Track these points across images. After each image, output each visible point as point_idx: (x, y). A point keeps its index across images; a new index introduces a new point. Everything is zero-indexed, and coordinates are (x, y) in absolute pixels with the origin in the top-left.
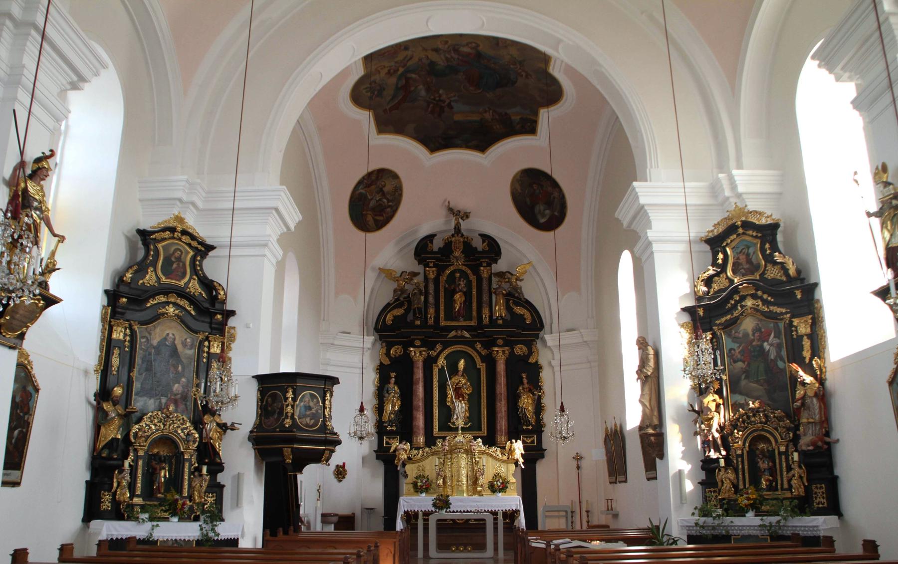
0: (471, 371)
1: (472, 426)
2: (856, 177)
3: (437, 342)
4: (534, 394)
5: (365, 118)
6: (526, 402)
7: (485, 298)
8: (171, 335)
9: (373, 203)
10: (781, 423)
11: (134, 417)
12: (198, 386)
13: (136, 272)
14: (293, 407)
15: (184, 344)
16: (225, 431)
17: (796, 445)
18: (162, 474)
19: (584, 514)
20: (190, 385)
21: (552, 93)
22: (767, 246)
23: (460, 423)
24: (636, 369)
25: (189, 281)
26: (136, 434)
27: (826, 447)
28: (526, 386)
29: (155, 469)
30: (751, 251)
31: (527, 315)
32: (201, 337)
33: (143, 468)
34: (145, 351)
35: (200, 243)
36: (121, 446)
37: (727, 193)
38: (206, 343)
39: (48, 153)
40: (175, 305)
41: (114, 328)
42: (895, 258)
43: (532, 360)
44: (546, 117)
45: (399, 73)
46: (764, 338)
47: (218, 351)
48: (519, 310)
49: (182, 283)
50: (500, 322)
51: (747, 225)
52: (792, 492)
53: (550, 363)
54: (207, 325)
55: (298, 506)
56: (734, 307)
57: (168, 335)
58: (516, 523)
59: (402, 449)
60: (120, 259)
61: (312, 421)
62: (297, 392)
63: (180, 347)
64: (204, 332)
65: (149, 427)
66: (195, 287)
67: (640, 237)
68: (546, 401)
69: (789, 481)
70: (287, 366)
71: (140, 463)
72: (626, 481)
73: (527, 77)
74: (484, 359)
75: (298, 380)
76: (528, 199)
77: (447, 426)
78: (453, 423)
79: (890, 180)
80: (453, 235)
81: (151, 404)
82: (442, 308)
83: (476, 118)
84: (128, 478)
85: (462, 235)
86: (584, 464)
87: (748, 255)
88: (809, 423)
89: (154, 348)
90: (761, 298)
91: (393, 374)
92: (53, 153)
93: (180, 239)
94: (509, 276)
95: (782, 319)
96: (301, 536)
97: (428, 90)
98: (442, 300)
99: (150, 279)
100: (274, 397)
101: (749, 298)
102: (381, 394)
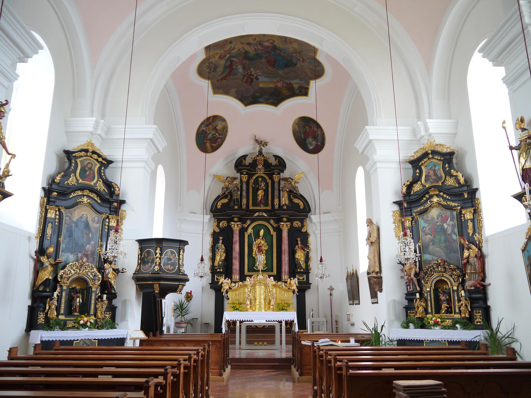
0: (267, 236)
1: (268, 269)
2: (504, 125)
3: (248, 219)
4: (304, 251)
5: (206, 85)
6: (300, 255)
7: (276, 193)
8: (85, 215)
9: (210, 135)
10: (454, 272)
11: (60, 266)
12: (101, 246)
13: (63, 176)
14: (160, 258)
15: (93, 220)
16: (118, 273)
17: (463, 286)
18: (78, 300)
19: (334, 323)
20: (97, 246)
21: (318, 71)
22: (447, 165)
23: (261, 268)
24: (366, 238)
25: (97, 182)
26: (62, 276)
27: (482, 287)
28: (300, 245)
29: (74, 298)
30: (437, 168)
31: (301, 204)
32: (104, 216)
33: (66, 298)
34: (68, 224)
35: (103, 159)
36: (52, 283)
37: (423, 133)
38: (107, 220)
39: (4, 102)
40: (88, 196)
41: (49, 211)
42: (527, 175)
43: (303, 230)
44: (313, 85)
45: (227, 57)
46: (445, 220)
47: (115, 225)
48: (296, 201)
49: (92, 183)
50: (285, 207)
51: (434, 153)
52: (461, 315)
53: (314, 232)
54: (108, 209)
55: (162, 318)
56: (426, 202)
57: (83, 215)
58: (293, 329)
59: (225, 282)
60: (53, 168)
61: (172, 267)
62: (163, 250)
63: (90, 223)
64: (106, 213)
65: (70, 272)
66: (100, 186)
67: (369, 159)
68: (311, 255)
69: (459, 308)
70: (158, 234)
71: (64, 294)
72: (359, 304)
73: (303, 61)
74: (275, 229)
75: (163, 242)
76: (302, 135)
77: (253, 269)
78: (257, 267)
79: (525, 127)
80: (258, 156)
81: (71, 257)
82: (251, 198)
83: (272, 86)
84: (56, 303)
85: (263, 156)
86: (334, 292)
87: (435, 171)
88: (472, 273)
89: (74, 223)
90: (442, 197)
91: (221, 238)
92: (7, 103)
93: (91, 157)
94: (291, 180)
95: (455, 210)
96: (164, 338)
97: (244, 68)
98: (251, 194)
99: (72, 181)
100: (149, 253)
101: (435, 197)
102: (214, 250)
